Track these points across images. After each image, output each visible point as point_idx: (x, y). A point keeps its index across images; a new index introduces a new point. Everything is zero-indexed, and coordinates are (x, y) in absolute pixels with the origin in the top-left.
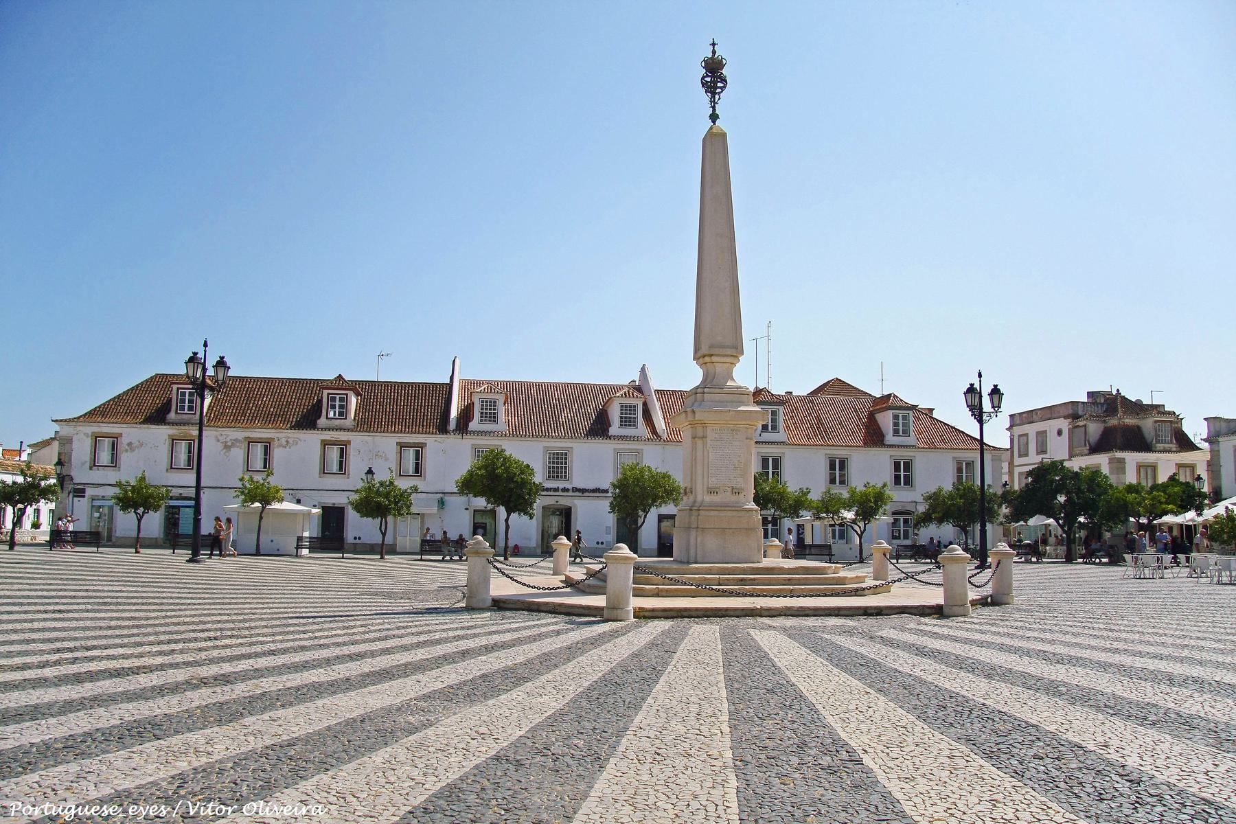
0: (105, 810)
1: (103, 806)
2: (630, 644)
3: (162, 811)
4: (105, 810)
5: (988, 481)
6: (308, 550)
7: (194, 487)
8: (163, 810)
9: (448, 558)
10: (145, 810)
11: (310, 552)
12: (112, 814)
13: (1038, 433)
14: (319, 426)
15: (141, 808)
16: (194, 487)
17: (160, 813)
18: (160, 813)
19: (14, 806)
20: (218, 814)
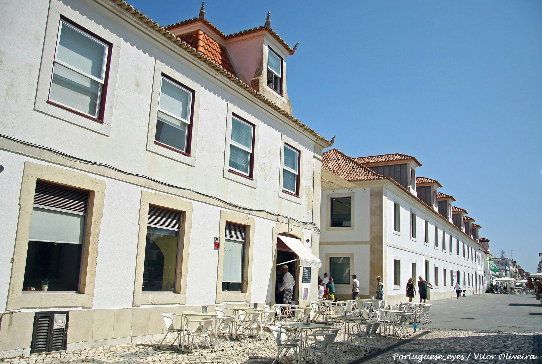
0: (436, 357)
1: (435, 356)
2: (455, 334)
3: (462, 358)
4: (436, 357)
5: (233, 332)
6: (82, 308)
7: (366, 243)
8: (463, 357)
9: (500, 281)
10: (454, 356)
11: (82, 308)
12: (439, 359)
13: (292, 309)
14: (76, 241)
15: (453, 356)
16: (366, 243)
17: (461, 358)
18: (461, 358)
19: (395, 355)
20: (487, 359)
